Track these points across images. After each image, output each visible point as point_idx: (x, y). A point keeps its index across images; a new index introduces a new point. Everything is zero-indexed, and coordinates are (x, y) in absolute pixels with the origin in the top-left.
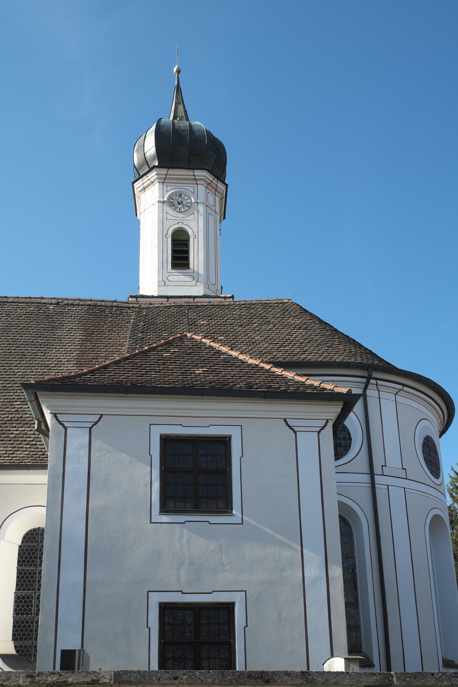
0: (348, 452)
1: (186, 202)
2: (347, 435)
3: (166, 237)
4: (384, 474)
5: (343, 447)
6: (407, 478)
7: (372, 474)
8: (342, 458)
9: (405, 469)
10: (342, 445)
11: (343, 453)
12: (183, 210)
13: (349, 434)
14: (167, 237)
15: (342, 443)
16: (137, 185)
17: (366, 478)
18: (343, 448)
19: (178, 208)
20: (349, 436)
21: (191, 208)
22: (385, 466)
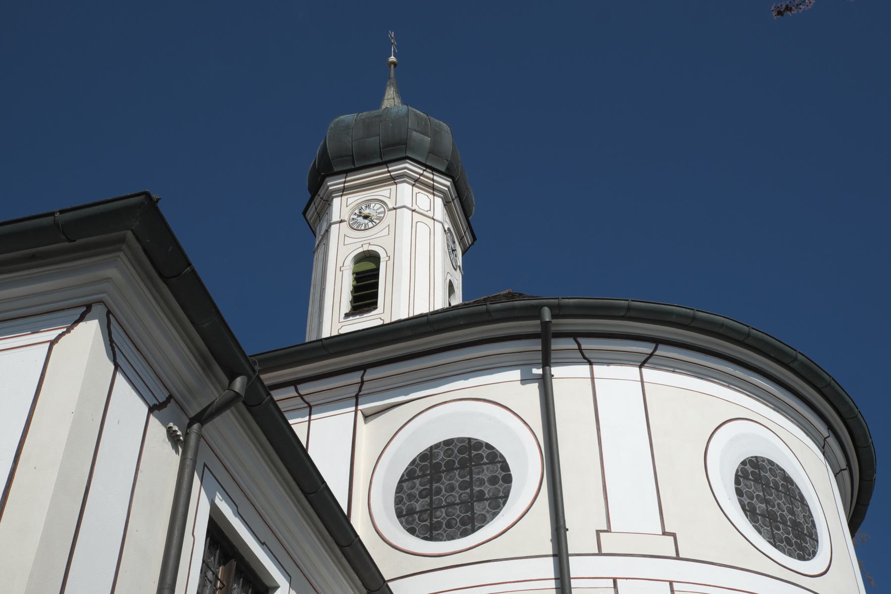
0: (501, 510)
1: (375, 210)
2: (499, 470)
4: (603, 552)
5: (487, 499)
6: (681, 556)
7: (560, 555)
8: (482, 526)
9: (674, 535)
10: (485, 495)
11: (488, 515)
12: (372, 225)
13: (505, 467)
15: (486, 492)
16: (309, 215)
17: (548, 567)
18: (487, 503)
19: (364, 225)
21: (383, 221)
22: (609, 531)
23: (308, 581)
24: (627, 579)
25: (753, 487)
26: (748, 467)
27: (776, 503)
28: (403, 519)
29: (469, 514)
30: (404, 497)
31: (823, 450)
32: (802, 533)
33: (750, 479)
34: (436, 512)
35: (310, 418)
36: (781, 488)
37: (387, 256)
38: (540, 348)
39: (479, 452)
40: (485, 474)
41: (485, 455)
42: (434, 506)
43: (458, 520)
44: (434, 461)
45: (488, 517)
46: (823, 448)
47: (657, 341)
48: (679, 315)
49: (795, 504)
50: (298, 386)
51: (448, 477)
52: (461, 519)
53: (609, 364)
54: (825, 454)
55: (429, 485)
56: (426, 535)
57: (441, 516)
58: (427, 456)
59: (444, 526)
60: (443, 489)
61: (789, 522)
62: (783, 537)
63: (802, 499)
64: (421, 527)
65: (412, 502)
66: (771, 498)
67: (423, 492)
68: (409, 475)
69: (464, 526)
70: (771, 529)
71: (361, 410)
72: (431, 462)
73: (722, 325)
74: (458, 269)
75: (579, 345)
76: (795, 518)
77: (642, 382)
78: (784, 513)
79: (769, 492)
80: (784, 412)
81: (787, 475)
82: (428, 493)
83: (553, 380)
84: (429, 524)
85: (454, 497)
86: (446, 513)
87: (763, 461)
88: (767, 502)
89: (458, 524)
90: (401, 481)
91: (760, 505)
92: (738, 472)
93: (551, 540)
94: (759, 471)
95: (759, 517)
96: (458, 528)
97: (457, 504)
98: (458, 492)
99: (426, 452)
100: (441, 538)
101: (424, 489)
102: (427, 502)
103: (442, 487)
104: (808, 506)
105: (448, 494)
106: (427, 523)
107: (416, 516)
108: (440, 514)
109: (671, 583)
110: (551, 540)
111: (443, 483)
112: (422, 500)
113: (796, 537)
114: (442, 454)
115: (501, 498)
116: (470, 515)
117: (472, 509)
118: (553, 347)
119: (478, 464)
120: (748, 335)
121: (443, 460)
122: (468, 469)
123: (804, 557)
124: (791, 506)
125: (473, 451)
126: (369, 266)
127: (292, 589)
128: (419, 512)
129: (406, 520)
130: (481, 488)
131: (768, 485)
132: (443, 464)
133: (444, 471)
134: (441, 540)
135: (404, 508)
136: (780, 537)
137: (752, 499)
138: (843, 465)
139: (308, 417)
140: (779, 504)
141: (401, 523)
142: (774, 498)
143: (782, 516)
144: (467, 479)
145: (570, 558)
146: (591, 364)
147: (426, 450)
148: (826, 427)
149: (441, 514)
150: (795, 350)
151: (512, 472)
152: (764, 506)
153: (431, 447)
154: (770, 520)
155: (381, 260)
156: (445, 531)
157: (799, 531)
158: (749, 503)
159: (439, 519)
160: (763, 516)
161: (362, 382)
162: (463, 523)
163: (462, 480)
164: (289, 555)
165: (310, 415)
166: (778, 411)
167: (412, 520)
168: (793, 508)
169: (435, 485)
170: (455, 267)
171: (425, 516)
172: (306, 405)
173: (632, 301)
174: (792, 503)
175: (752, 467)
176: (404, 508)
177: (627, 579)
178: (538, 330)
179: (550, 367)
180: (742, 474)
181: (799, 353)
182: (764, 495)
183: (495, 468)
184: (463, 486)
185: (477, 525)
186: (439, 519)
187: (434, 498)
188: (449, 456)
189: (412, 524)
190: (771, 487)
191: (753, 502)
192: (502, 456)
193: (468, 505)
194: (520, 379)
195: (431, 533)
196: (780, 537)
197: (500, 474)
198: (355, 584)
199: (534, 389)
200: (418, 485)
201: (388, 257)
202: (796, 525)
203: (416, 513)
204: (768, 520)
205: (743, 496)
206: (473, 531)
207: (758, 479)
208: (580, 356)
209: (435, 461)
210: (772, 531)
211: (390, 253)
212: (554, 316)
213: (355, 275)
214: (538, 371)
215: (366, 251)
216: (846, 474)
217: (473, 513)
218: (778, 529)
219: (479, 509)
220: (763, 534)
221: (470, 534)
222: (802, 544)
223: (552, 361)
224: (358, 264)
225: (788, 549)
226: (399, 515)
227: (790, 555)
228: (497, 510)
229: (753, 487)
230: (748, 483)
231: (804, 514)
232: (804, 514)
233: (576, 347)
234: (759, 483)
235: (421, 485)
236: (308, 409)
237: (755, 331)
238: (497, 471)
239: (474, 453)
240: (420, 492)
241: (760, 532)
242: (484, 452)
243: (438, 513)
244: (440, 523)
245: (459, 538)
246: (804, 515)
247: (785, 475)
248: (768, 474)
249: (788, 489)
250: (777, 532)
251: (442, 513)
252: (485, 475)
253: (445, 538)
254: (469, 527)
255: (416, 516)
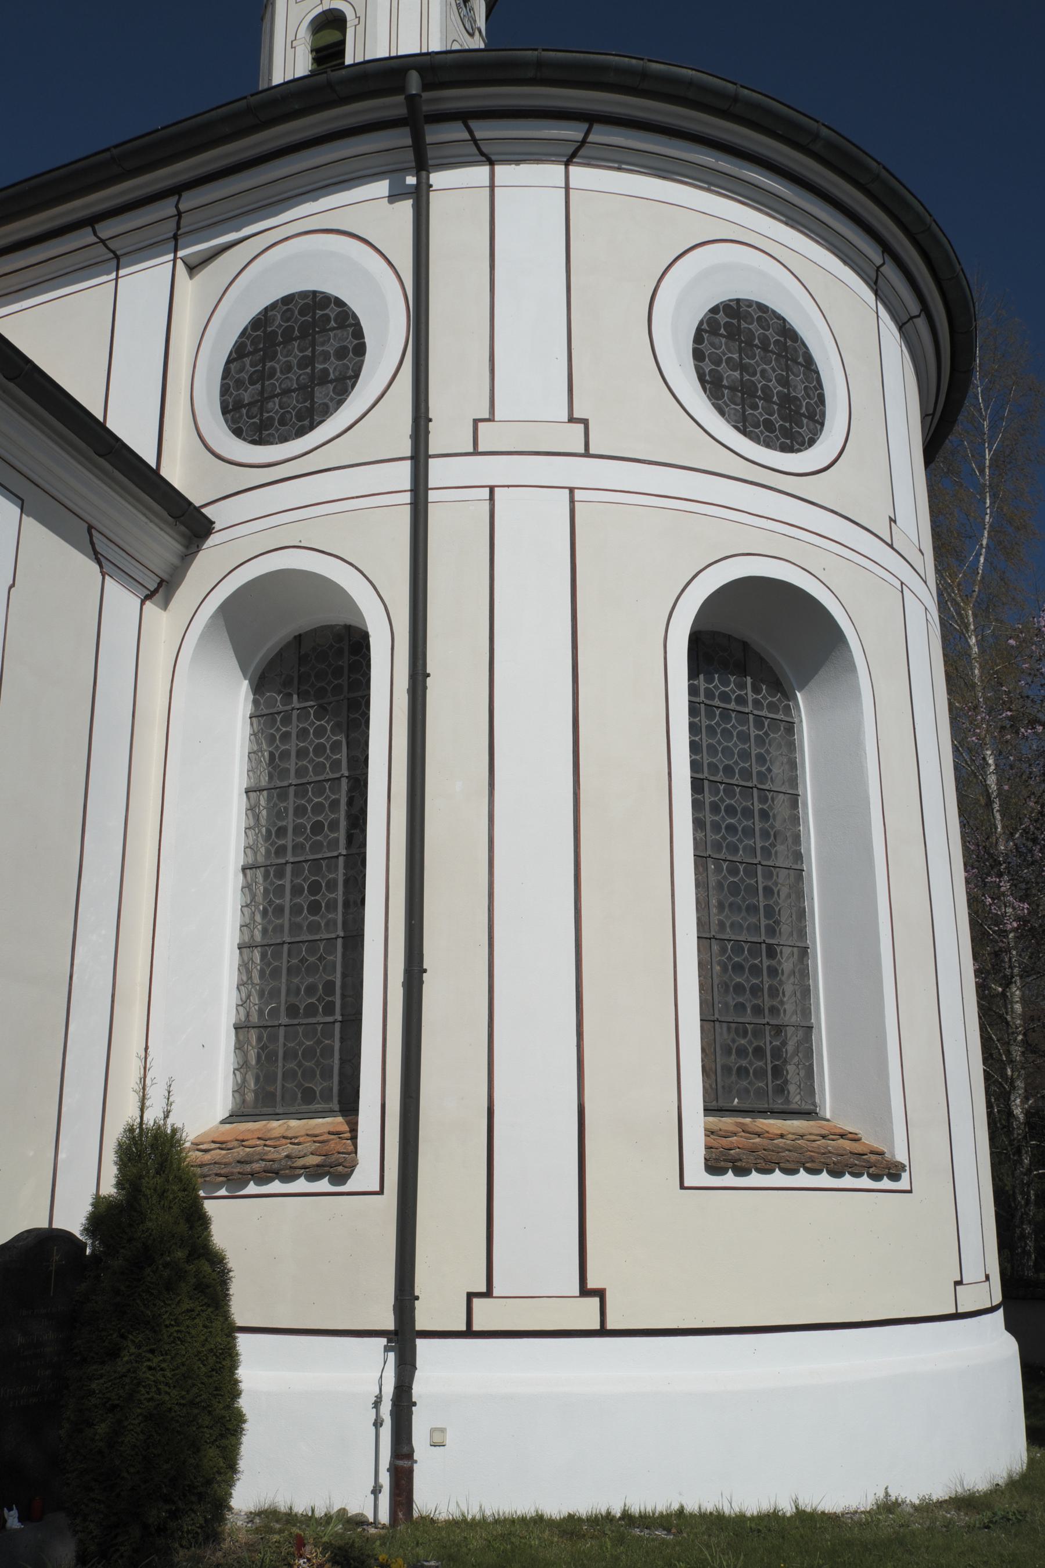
0: (348, 396)
3: (585, 422)
5: (331, 382)
8: (323, 421)
10: (329, 374)
11: (331, 404)
13: (358, 333)
14: (572, 420)
15: (331, 371)
17: (402, 474)
18: (331, 387)
20: (356, 342)
23: (63, 505)
24: (508, 486)
25: (723, 347)
26: (722, 319)
27: (759, 370)
28: (229, 416)
29: (307, 404)
30: (231, 384)
31: (875, 287)
32: (797, 412)
33: (722, 335)
34: (267, 403)
35: (117, 275)
36: (772, 346)
37: (356, 17)
38: (409, 141)
39: (325, 312)
40: (332, 345)
41: (332, 316)
42: (265, 396)
43: (294, 414)
44: (269, 329)
45: (331, 407)
46: (876, 283)
47: (591, 119)
48: (618, 70)
49: (795, 370)
50: (97, 226)
51: (285, 352)
52: (298, 411)
53: (518, 162)
54: (879, 292)
55: (261, 365)
56: (254, 437)
57: (273, 409)
58: (259, 322)
59: (276, 423)
60: (278, 370)
61: (775, 397)
62: (761, 420)
63: (809, 363)
64: (249, 426)
65: (241, 391)
66: (752, 362)
67: (254, 376)
68: (238, 353)
69: (300, 421)
70: (743, 408)
71: (181, 258)
72: (265, 332)
73: (691, 83)
74: (477, 33)
75: (471, 132)
76: (789, 390)
77: (567, 188)
78: (770, 384)
79: (750, 353)
80: (805, 227)
81: (788, 326)
82: (259, 377)
83: (431, 193)
84: (258, 421)
85: (291, 380)
86: (279, 405)
87: (750, 306)
88: (743, 368)
89: (294, 419)
90: (229, 361)
91: (732, 373)
92: (703, 325)
93: (411, 437)
94: (739, 321)
95: (726, 391)
96: (293, 425)
97: (294, 391)
98: (295, 373)
99: (259, 317)
100: (272, 440)
101: (255, 372)
102: (257, 389)
103: (277, 366)
104: (817, 373)
105: (284, 377)
106: (256, 420)
107: (244, 411)
108: (273, 406)
109: (572, 490)
110: (410, 436)
111: (278, 362)
112: (252, 387)
113: (782, 419)
114: (279, 317)
115: (350, 378)
116: (309, 406)
117: (311, 396)
118: (429, 139)
119: (324, 330)
120: (735, 99)
121: (280, 326)
122: (310, 338)
123: (793, 446)
124: (784, 373)
125: (317, 311)
126: (330, 37)
127: (28, 515)
128: (248, 404)
129: (232, 417)
130: (326, 366)
131: (750, 343)
132: (280, 332)
133: (281, 343)
134: (272, 444)
135: (230, 401)
136: (756, 419)
137: (718, 363)
138: (914, 308)
139: (115, 273)
140: (763, 371)
141: (226, 421)
142: (756, 362)
143: (765, 388)
144: (308, 353)
145: (431, 461)
146: (492, 163)
147: (260, 313)
148: (880, 250)
149: (274, 405)
150: (817, 122)
151: (367, 340)
152: (737, 374)
153: (266, 309)
154: (743, 395)
155: (349, 24)
156: (277, 430)
157: (791, 410)
158: (711, 371)
159: (271, 414)
160: (732, 389)
161: (179, 214)
162: (300, 418)
163: (302, 354)
164: (7, 462)
165: (118, 270)
166: (792, 227)
167: (239, 417)
168: (788, 376)
169: (269, 365)
170: (471, 31)
171: (255, 410)
172: (111, 255)
173: (544, 50)
174: (788, 368)
175: (727, 315)
176: (230, 401)
177: (508, 486)
178: (402, 111)
179: (429, 173)
180: (708, 327)
181: (824, 125)
182: (741, 358)
183: (345, 333)
184: (303, 364)
185: (317, 418)
186: (271, 414)
187: (267, 383)
188: (288, 320)
189: (239, 423)
190: (756, 346)
191: (719, 369)
192: (355, 317)
193: (306, 391)
194: (387, 195)
195: (259, 435)
196: (756, 419)
197: (351, 343)
198: (149, 508)
199: (406, 207)
200: (248, 366)
201: (357, 19)
202: (787, 400)
203: (244, 406)
204: (740, 394)
205: (705, 361)
206: (312, 427)
207: (733, 334)
208: (475, 151)
209: (271, 329)
210: (744, 411)
211: (361, 13)
212: (426, 86)
213: (314, 53)
214: (411, 180)
215: (326, 10)
216: (921, 323)
217: (313, 402)
218: (755, 407)
219: (321, 395)
220: (727, 415)
221: (307, 433)
222: (792, 428)
223: (430, 162)
224: (317, 35)
225: (767, 436)
226: (225, 411)
227: (768, 445)
228: (343, 397)
229: (723, 347)
230: (716, 340)
231: (807, 384)
232: (807, 384)
233: (466, 135)
234: (736, 340)
235: (251, 366)
236: (115, 262)
237: (746, 91)
238: (347, 338)
239: (319, 313)
240: (250, 377)
241: (722, 413)
242: (332, 311)
243: (270, 405)
244: (271, 418)
245: (294, 439)
246: (806, 387)
247: (785, 326)
248: (754, 326)
249: (785, 348)
250: (752, 412)
251: (275, 404)
252: (331, 348)
253: (277, 440)
254: (306, 422)
255: (244, 411)
